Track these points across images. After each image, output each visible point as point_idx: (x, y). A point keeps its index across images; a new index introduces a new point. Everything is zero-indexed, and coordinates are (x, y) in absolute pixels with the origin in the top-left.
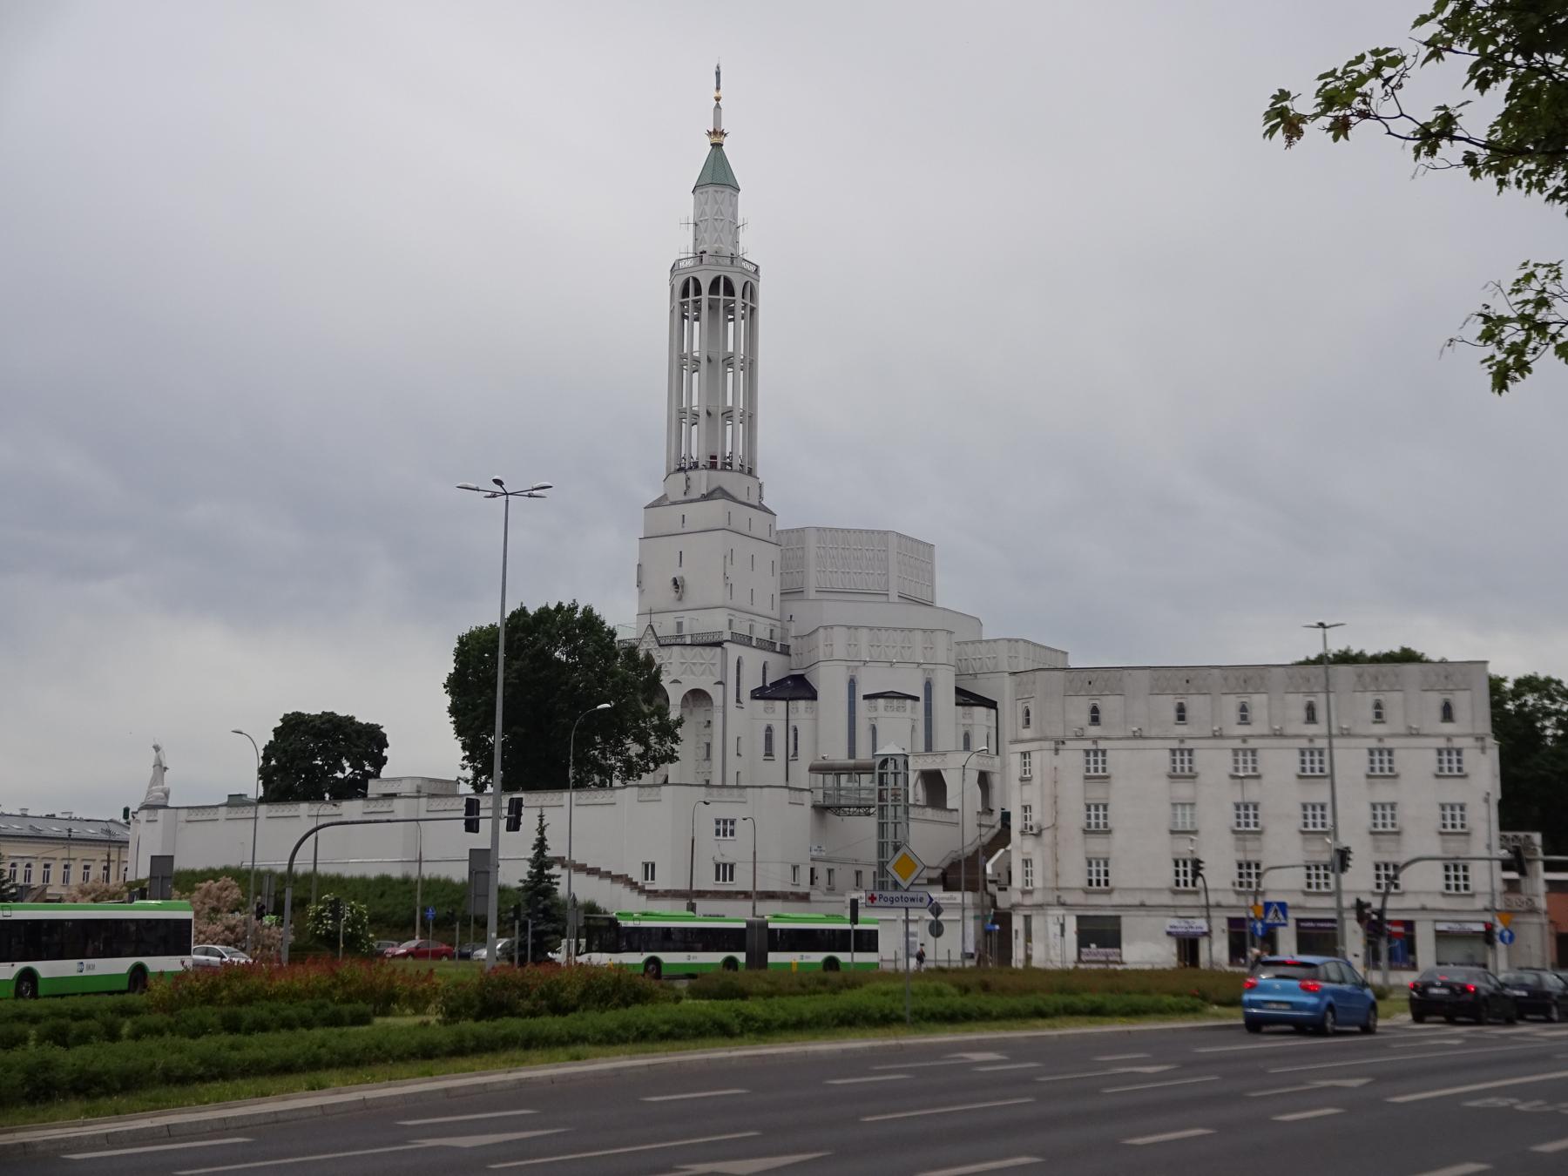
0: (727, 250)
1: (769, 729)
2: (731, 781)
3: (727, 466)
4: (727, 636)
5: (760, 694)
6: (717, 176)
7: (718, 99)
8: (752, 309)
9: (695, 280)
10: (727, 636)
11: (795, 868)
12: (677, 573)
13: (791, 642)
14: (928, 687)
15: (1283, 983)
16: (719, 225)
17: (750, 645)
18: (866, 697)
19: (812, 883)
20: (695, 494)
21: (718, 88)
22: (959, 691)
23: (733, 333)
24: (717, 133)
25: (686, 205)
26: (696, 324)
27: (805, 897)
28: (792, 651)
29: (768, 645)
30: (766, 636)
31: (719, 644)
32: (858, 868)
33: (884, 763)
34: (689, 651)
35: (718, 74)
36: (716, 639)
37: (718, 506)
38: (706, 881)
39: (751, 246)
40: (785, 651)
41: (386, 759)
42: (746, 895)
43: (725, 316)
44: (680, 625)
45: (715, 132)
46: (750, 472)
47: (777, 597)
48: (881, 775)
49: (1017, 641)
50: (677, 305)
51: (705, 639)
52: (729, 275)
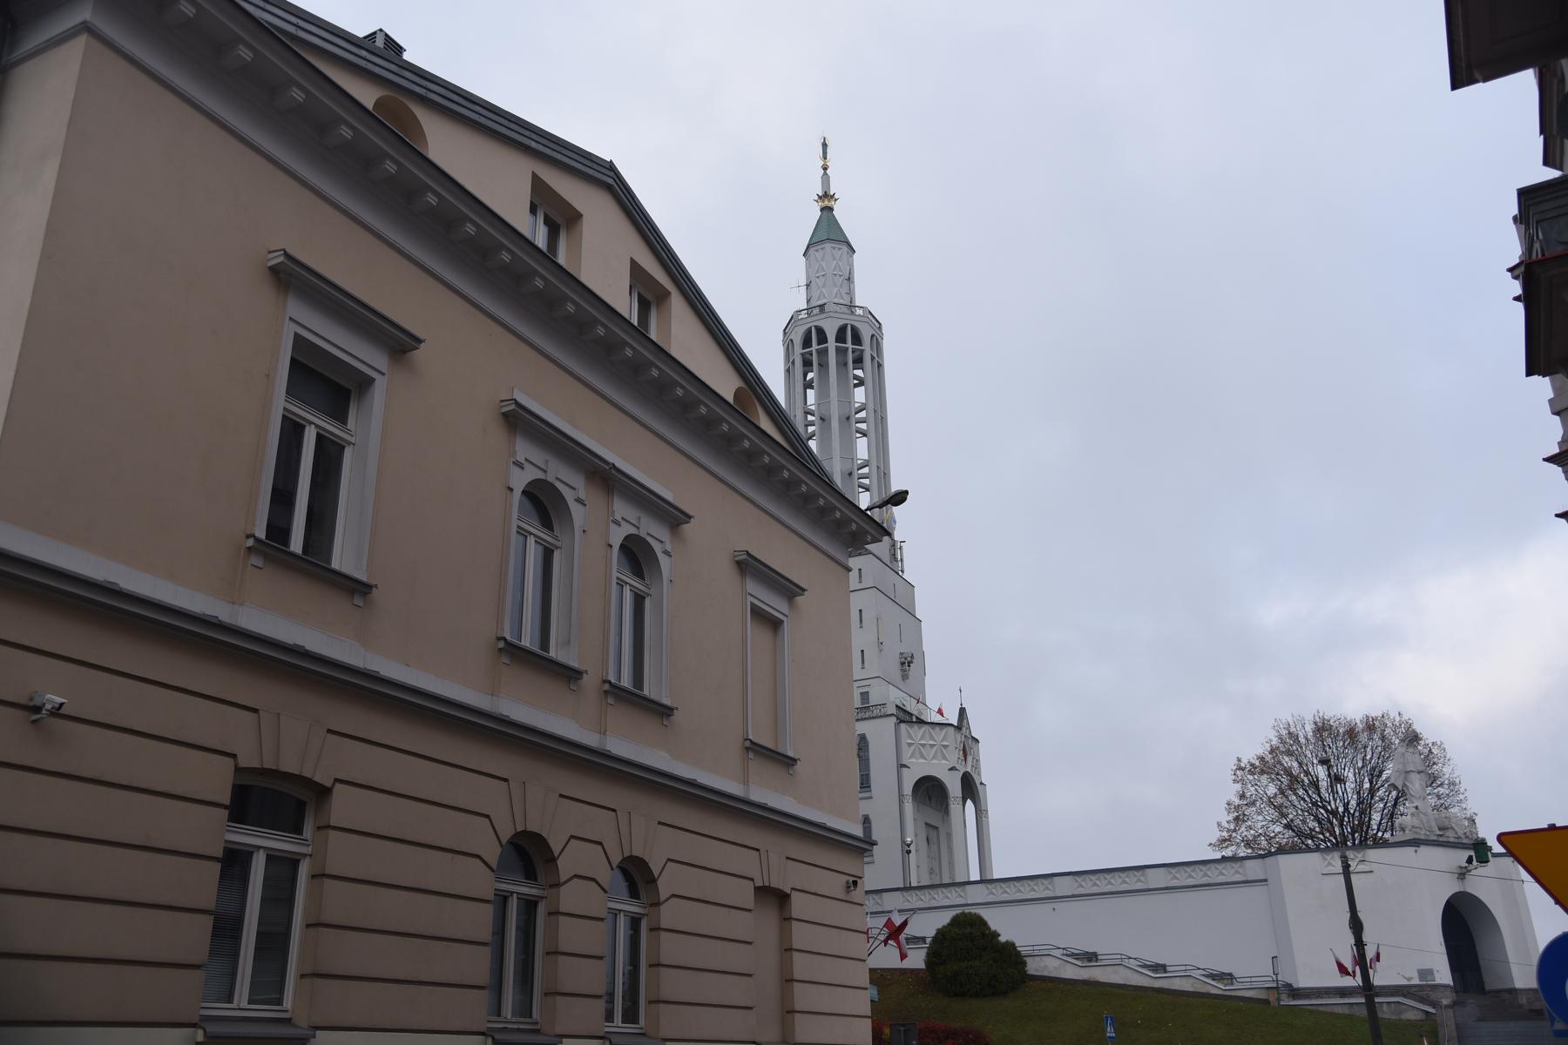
6: (828, 234)
7: (825, 169)
8: (880, 366)
9: (854, 329)
24: (826, 196)
25: (798, 270)
35: (825, 145)
39: (872, 292)
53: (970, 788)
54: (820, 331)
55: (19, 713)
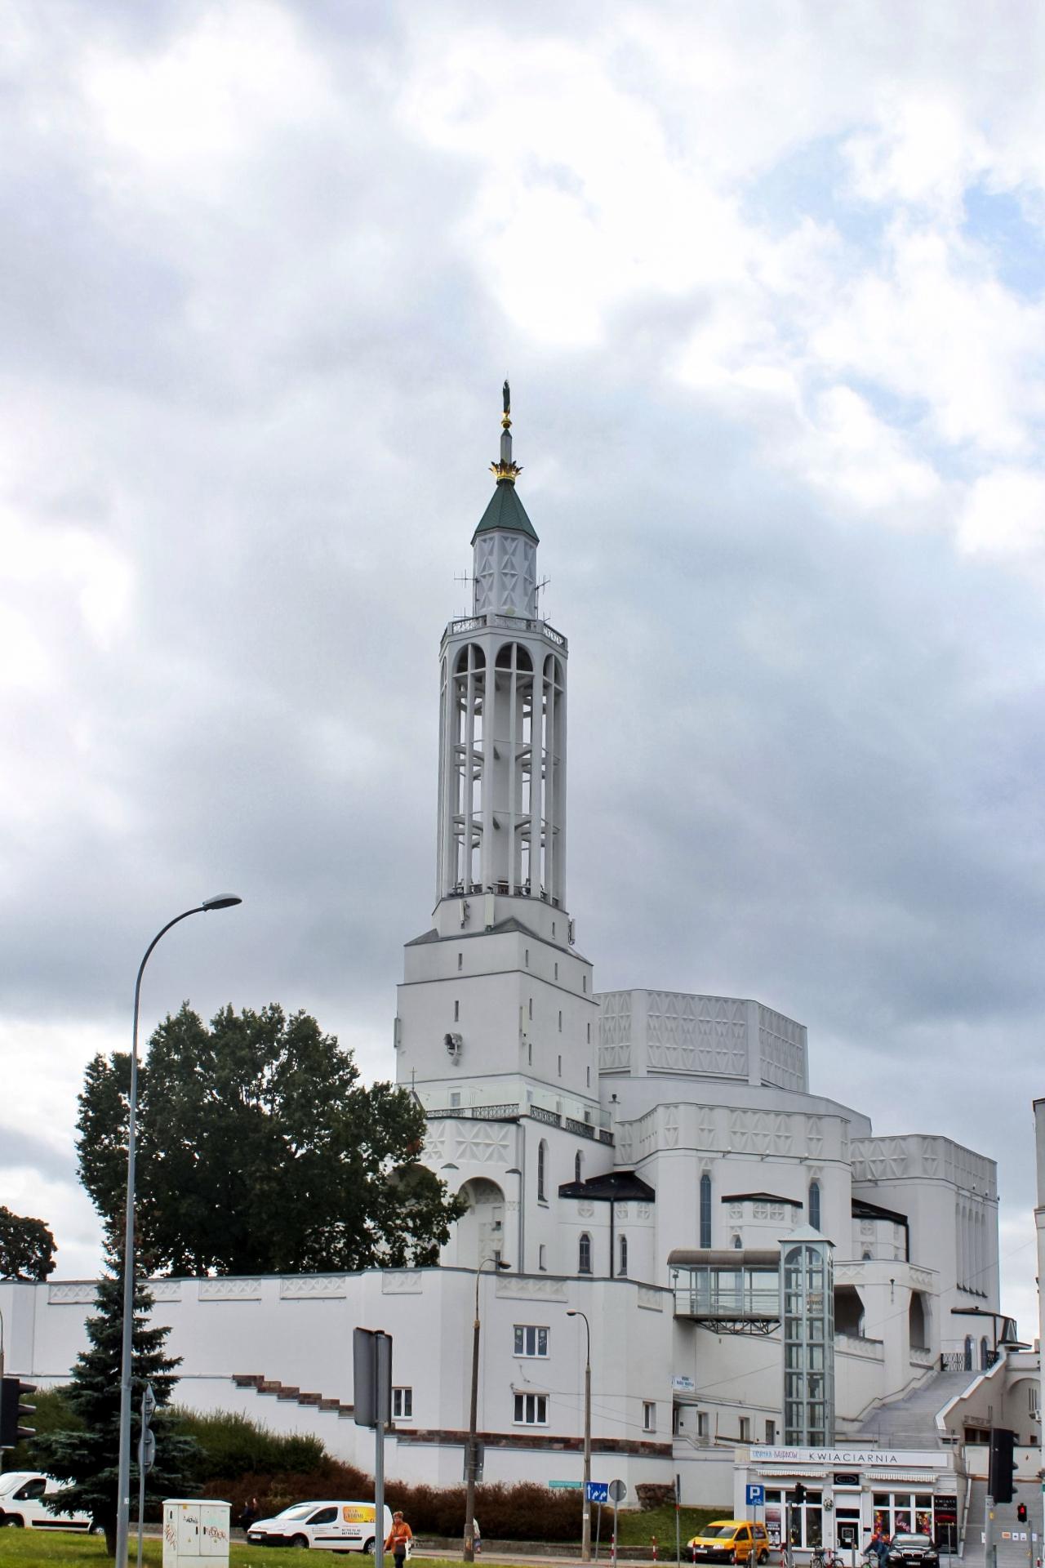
0: (521, 611)
1: (585, 1238)
2: (531, 1268)
3: (523, 893)
4: (524, 1109)
5: (570, 1191)
6: (506, 518)
7: (507, 424)
8: (559, 695)
11: (648, 1406)
12: (454, 1029)
13: (614, 1129)
14: (814, 1191)
15: (410, 1498)
16: (508, 580)
18: (726, 1199)
19: (675, 1431)
20: (477, 926)
21: (507, 411)
22: (856, 1203)
26: (478, 719)
27: (664, 1452)
28: (617, 1141)
29: (584, 1130)
30: (580, 1118)
31: (513, 1120)
32: (744, 1413)
33: (793, 1256)
34: (470, 1131)
35: (506, 392)
36: (509, 1113)
37: (510, 942)
38: (498, 1418)
39: (551, 609)
40: (607, 1139)
41: (53, 1265)
42: (569, 1445)
43: (519, 708)
44: (455, 1097)
46: (557, 904)
47: (594, 1073)
48: (788, 1273)
49: (935, 1138)
50: (448, 682)
51: (492, 1114)
54: (478, 650)
55: (694, 1108)
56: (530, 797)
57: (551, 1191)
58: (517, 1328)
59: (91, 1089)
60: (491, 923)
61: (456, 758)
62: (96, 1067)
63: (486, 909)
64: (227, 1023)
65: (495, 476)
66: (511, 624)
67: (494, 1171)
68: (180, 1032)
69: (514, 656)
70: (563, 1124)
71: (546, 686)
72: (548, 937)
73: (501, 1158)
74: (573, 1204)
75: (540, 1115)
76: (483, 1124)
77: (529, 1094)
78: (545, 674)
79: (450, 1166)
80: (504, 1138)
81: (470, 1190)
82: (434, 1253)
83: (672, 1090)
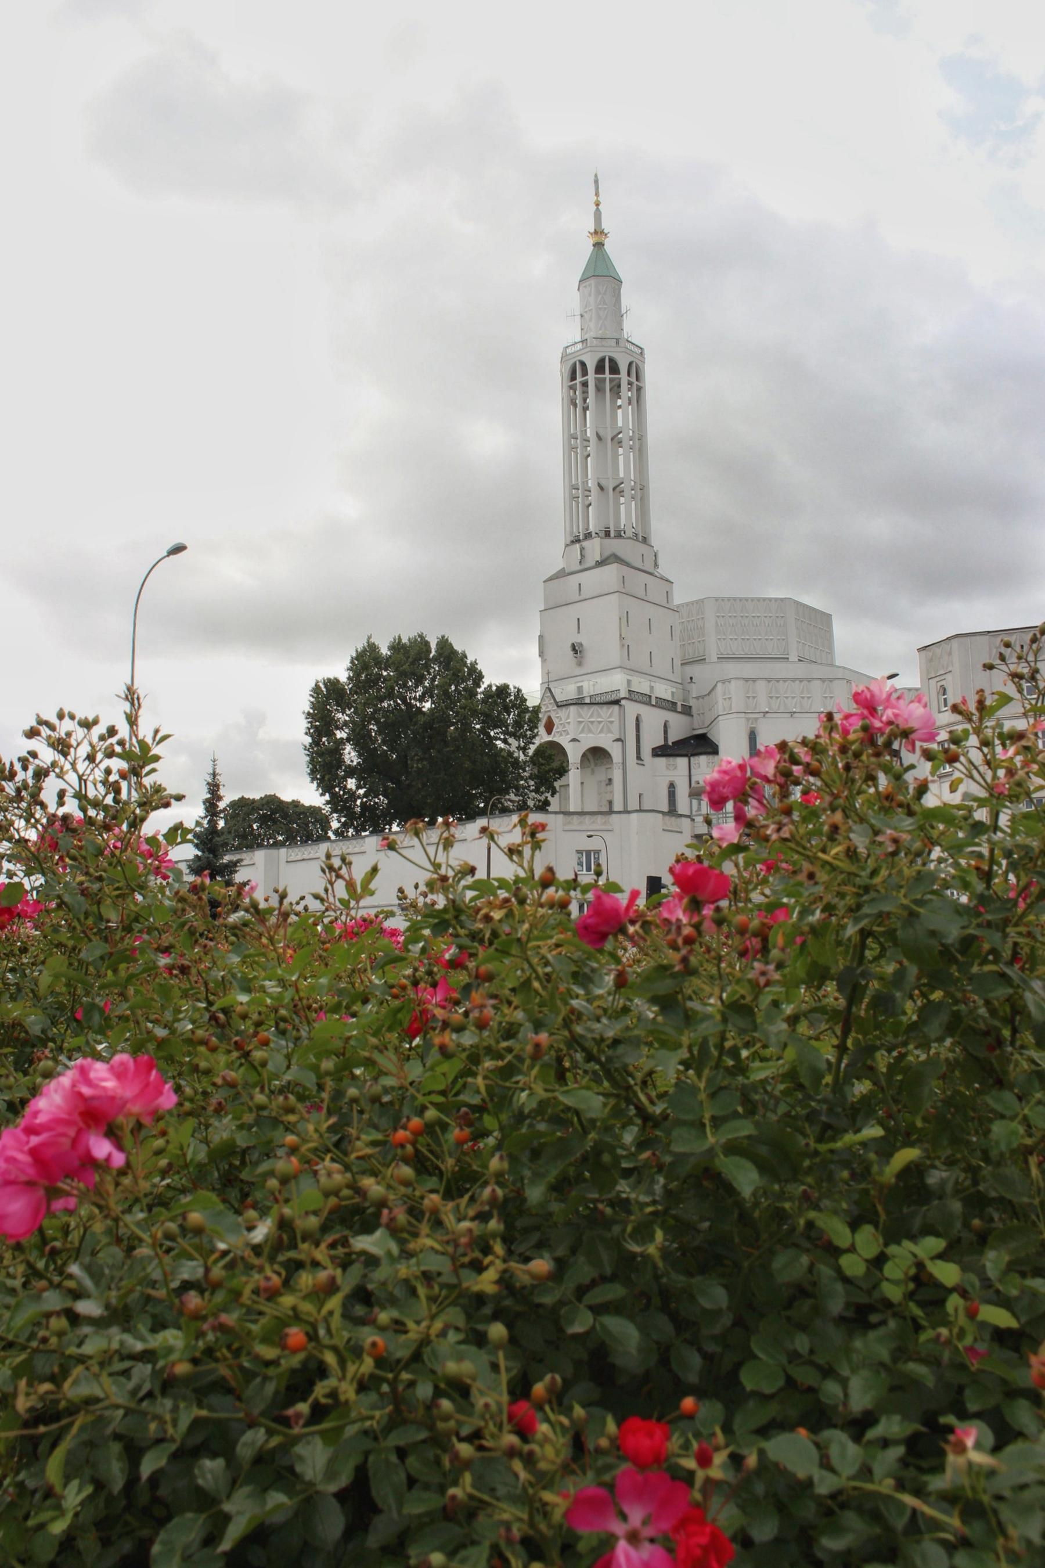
4: (623, 694)
5: (662, 751)
7: (597, 205)
8: (639, 389)
9: (611, 360)
10: (623, 694)
12: (577, 639)
13: (692, 703)
17: (649, 704)
20: (590, 562)
21: (597, 194)
23: (624, 417)
24: (598, 232)
25: (573, 300)
28: (694, 711)
31: (617, 702)
34: (586, 712)
35: (596, 182)
36: (614, 697)
37: (611, 571)
40: (687, 711)
44: (580, 689)
45: (596, 232)
46: (645, 540)
47: (677, 663)
51: (604, 699)
52: (614, 355)
53: (323, 871)
54: (583, 364)
56: (624, 465)
57: (647, 752)
58: (578, 852)
59: (314, 706)
60: (598, 559)
61: (575, 443)
62: (316, 689)
63: (595, 548)
64: (397, 647)
65: (591, 241)
66: (604, 343)
67: (604, 741)
68: (366, 661)
69: (607, 366)
70: (653, 702)
71: (630, 383)
72: (639, 565)
73: (610, 731)
74: (662, 761)
75: (633, 696)
76: (595, 707)
77: (629, 682)
78: (629, 375)
79: (574, 740)
80: (611, 716)
81: (590, 756)
82: (547, 803)
83: (732, 669)
